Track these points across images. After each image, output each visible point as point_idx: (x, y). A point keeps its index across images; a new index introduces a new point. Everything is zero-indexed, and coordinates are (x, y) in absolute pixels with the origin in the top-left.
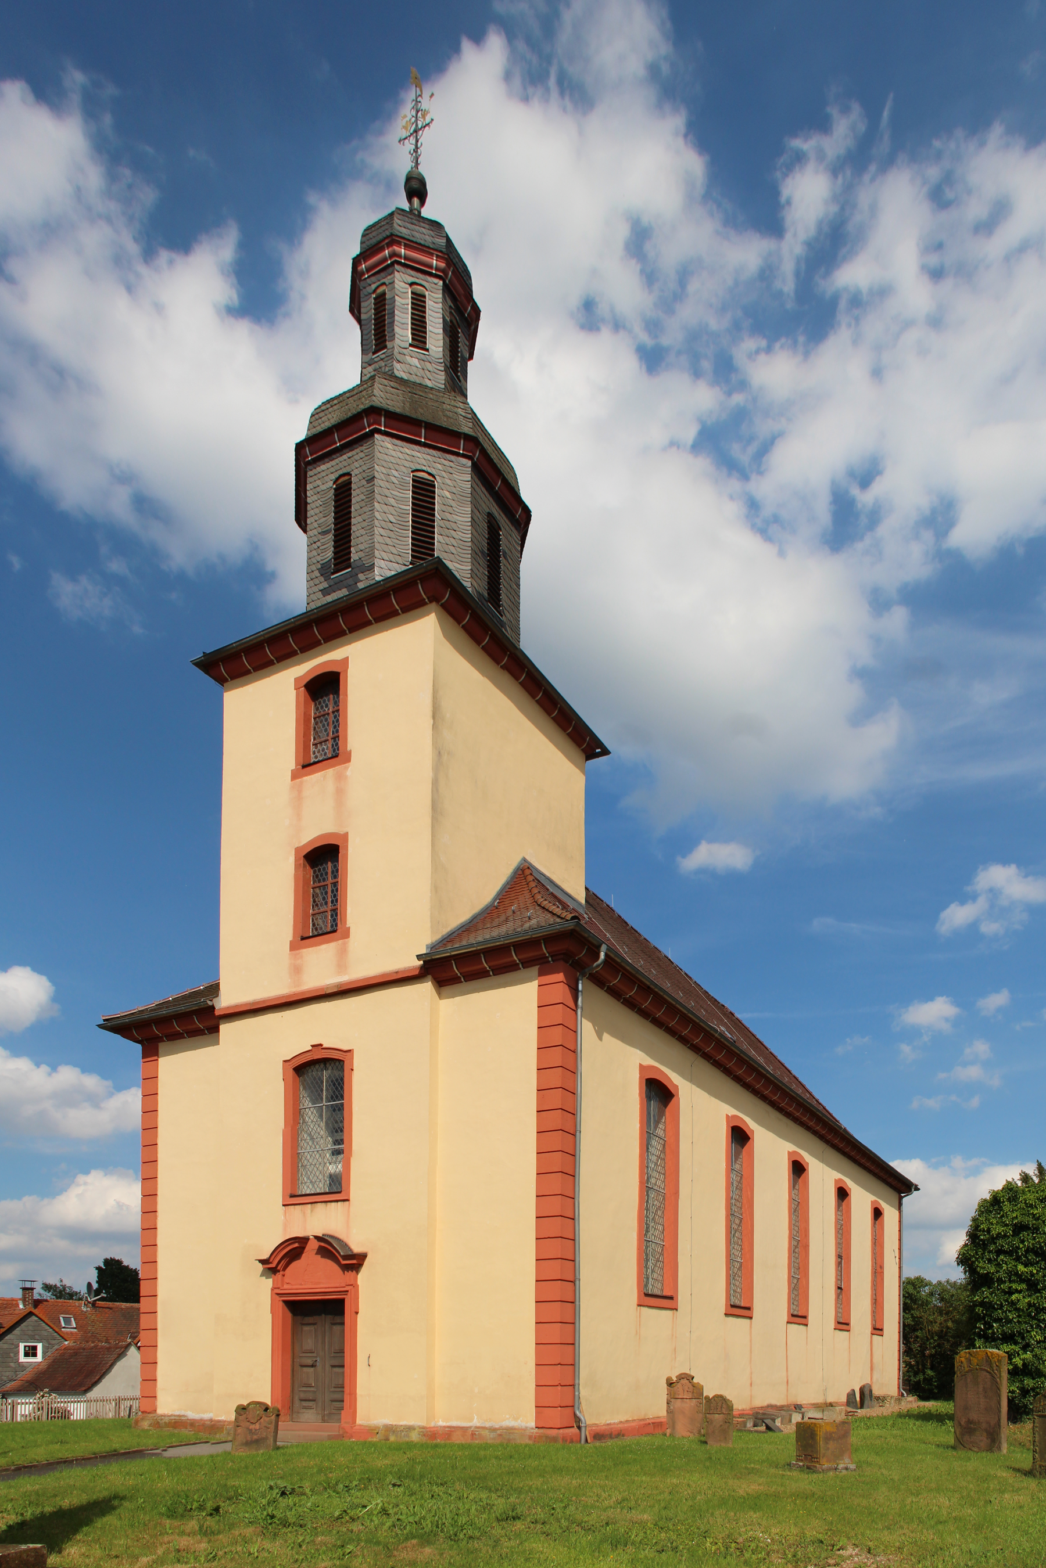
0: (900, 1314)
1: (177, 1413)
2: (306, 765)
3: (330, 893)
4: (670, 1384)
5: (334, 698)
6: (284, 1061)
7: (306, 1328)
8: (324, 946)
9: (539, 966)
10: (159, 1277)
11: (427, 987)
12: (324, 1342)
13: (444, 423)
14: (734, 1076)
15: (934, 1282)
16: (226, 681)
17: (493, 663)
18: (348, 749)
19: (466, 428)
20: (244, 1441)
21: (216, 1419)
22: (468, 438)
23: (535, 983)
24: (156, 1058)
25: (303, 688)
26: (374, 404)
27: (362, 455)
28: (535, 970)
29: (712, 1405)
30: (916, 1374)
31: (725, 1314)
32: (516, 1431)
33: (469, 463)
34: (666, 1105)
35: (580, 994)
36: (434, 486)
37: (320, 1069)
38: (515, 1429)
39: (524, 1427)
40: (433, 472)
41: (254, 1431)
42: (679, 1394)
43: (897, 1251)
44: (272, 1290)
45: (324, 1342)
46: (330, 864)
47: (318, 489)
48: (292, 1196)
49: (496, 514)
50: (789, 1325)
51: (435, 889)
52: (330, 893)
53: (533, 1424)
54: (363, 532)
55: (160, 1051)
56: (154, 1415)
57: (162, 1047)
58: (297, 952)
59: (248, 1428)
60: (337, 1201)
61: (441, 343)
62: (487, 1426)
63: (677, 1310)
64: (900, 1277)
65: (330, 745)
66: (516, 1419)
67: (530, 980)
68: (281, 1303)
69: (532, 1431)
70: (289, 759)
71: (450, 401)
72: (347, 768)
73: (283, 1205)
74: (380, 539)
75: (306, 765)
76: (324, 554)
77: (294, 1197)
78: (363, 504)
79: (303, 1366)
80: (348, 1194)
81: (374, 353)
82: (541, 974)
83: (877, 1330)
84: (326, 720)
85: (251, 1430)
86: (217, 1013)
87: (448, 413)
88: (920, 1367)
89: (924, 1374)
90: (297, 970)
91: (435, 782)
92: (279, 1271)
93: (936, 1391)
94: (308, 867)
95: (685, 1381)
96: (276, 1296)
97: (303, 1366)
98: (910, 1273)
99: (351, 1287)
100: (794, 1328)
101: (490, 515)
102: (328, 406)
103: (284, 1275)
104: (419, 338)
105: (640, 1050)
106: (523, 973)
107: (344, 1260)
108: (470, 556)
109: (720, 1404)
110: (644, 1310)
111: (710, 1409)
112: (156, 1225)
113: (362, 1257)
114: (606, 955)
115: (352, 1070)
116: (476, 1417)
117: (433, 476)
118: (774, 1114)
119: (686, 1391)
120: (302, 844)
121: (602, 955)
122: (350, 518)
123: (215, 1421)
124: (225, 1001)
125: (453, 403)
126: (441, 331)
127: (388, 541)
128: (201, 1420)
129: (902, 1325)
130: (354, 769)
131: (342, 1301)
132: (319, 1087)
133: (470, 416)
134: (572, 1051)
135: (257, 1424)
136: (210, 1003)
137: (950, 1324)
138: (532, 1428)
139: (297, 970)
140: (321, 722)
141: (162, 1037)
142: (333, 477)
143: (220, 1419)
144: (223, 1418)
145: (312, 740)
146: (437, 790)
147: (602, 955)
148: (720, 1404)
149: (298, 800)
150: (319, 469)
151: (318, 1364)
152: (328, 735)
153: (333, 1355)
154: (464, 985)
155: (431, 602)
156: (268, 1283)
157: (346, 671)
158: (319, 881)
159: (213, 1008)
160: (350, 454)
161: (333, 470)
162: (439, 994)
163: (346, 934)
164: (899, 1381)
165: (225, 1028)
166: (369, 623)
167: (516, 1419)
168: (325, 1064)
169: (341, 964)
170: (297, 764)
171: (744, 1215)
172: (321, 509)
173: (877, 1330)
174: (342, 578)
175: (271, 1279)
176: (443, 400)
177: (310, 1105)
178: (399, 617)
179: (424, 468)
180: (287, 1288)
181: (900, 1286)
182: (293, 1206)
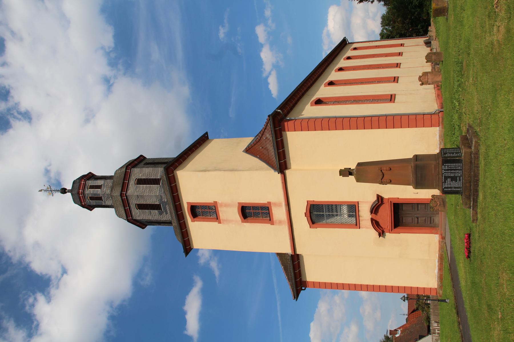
0: (395, 40)
1: (437, 279)
2: (217, 219)
3: (256, 211)
4: (422, 84)
5: (197, 209)
6: (310, 227)
7: (404, 221)
8: (273, 212)
9: (282, 132)
10: (385, 285)
11: (287, 172)
12: (409, 214)
13: (123, 175)
14: (310, 86)
15: (381, 28)
16: (190, 247)
17: (186, 159)
18: (213, 202)
19: (124, 169)
20: (443, 207)
21: (438, 258)
22: (126, 169)
23: (287, 133)
24: (307, 282)
26: (119, 195)
27: (131, 200)
28: (283, 133)
29: (429, 60)
30: (420, 32)
31: (397, 83)
32: (441, 134)
33: (132, 169)
34: (323, 102)
35: (291, 118)
36: (139, 179)
37: (313, 215)
38: (440, 135)
39: (439, 132)
40: (135, 179)
41: (440, 204)
42: (426, 81)
43: (369, 43)
44: (390, 233)
45: (409, 214)
46: (247, 211)
47: (139, 215)
48: (356, 225)
49: (143, 163)
50: (401, 68)
51: (257, 170)
52: (256, 211)
53: (438, 128)
54: (151, 200)
55: (305, 280)
56: (437, 289)
57: (303, 280)
58: (274, 222)
59: (439, 206)
60: (358, 206)
61: (100, 181)
62: (439, 146)
63: (395, 94)
64: (380, 41)
65: (211, 210)
67: (286, 134)
68: (395, 229)
69: (440, 127)
70: (214, 225)
71: (115, 179)
73: (360, 229)
74: (154, 194)
75: (217, 219)
77: (357, 225)
78: (144, 199)
79: (418, 223)
80: (356, 202)
81: (103, 201)
82: (285, 131)
83: (402, 45)
84: (203, 212)
85: (439, 205)
86: (293, 254)
87: (120, 174)
88: (417, 31)
89: (420, 29)
90: (280, 222)
91: (224, 171)
92: (383, 230)
93: (427, 24)
94: (248, 219)
95: (421, 78)
96: (392, 231)
97: (418, 223)
98: (379, 38)
99: (389, 200)
100: (401, 66)
101: (144, 164)
102: (118, 212)
103: (385, 229)
104: (99, 187)
105: (306, 106)
106: (284, 138)
107: (379, 202)
108: (157, 168)
109: (429, 57)
110: (395, 101)
111: (431, 60)
112: (366, 285)
113: (378, 196)
114: (279, 110)
115: (314, 201)
116: (436, 151)
117: (136, 179)
118: (322, 76)
119: (425, 78)
121: (279, 111)
122: (147, 204)
123: (439, 258)
124: (289, 251)
125: (117, 174)
126: (97, 181)
127: (154, 191)
128: (438, 266)
129: (399, 38)
130: (219, 201)
131: (394, 204)
132: (319, 215)
133: (120, 169)
134: (309, 119)
135: (438, 202)
136: (290, 255)
137: (399, 20)
138: (439, 128)
139: (280, 222)
140: (204, 214)
141: (300, 278)
142: (136, 210)
143: (438, 256)
144: (437, 255)
145: (209, 217)
146: (227, 170)
147: (279, 111)
148: (429, 57)
149: (228, 221)
150: (134, 215)
151: (417, 216)
152: (208, 211)
153: (414, 210)
154: (287, 159)
155: (173, 173)
156: (387, 234)
157: (190, 203)
158: (252, 215)
159: (292, 255)
160: (131, 204)
161: (134, 210)
162: (289, 169)
163: (269, 203)
164: (423, 38)
165: (298, 252)
166: (178, 194)
167: (436, 135)
168: (311, 213)
169: (278, 205)
170: (216, 222)
171: (359, 82)
172: (144, 214)
173: (402, 45)
174: (163, 207)
175: (386, 233)
176: (117, 177)
177: (325, 221)
178: (177, 184)
179: (134, 181)
180: (389, 227)
181: (384, 41)
182: (360, 225)
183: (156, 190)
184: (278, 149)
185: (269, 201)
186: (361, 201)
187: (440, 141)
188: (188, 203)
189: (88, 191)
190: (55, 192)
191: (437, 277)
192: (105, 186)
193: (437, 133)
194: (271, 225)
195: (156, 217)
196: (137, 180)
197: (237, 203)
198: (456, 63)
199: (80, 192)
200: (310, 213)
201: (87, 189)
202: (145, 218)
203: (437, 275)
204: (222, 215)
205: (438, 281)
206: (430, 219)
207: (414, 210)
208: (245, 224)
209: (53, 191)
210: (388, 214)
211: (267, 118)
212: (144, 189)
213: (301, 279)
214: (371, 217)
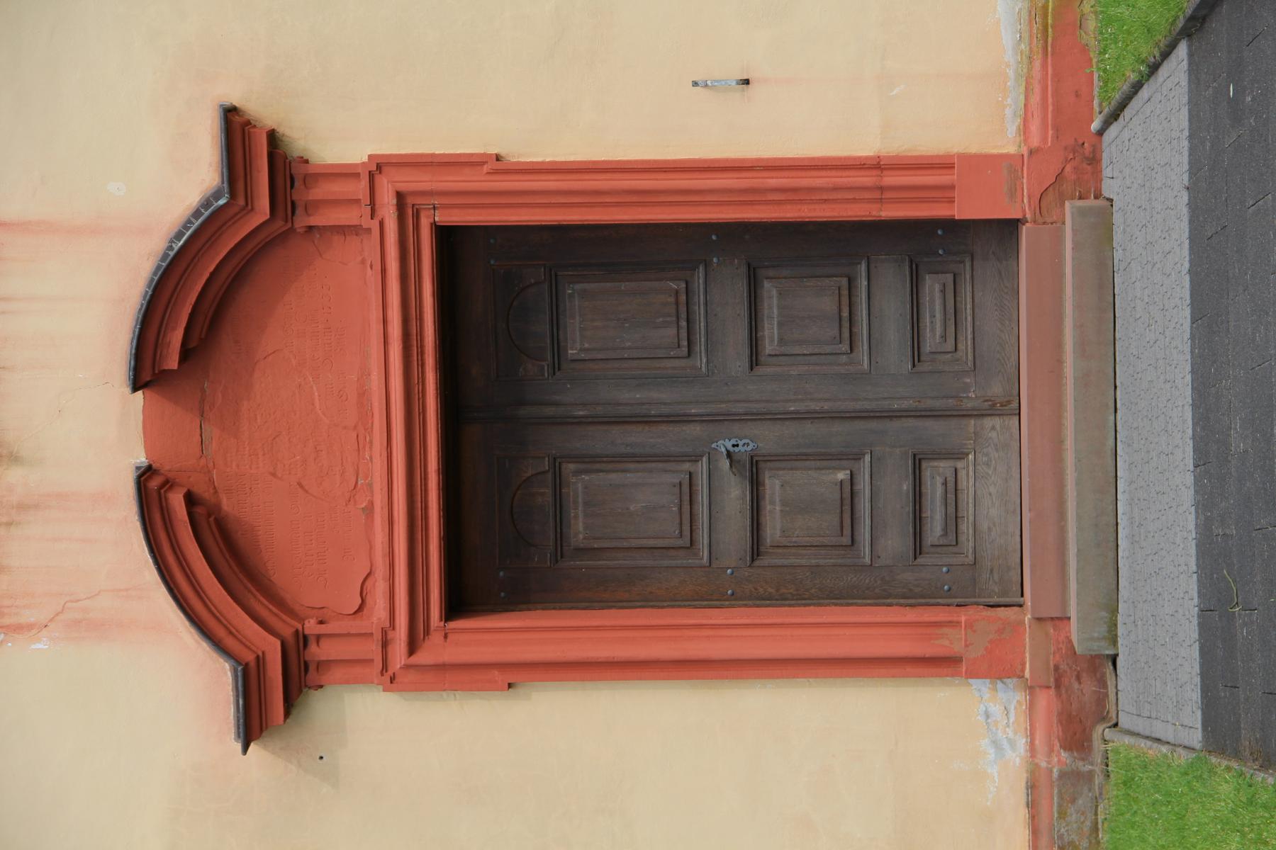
79: (756, 548)
107: (249, 207)
131: (447, 237)
198: (1125, 634)
206: (906, 486)
207: (701, 361)
210: (363, 394)
214: (142, 460)
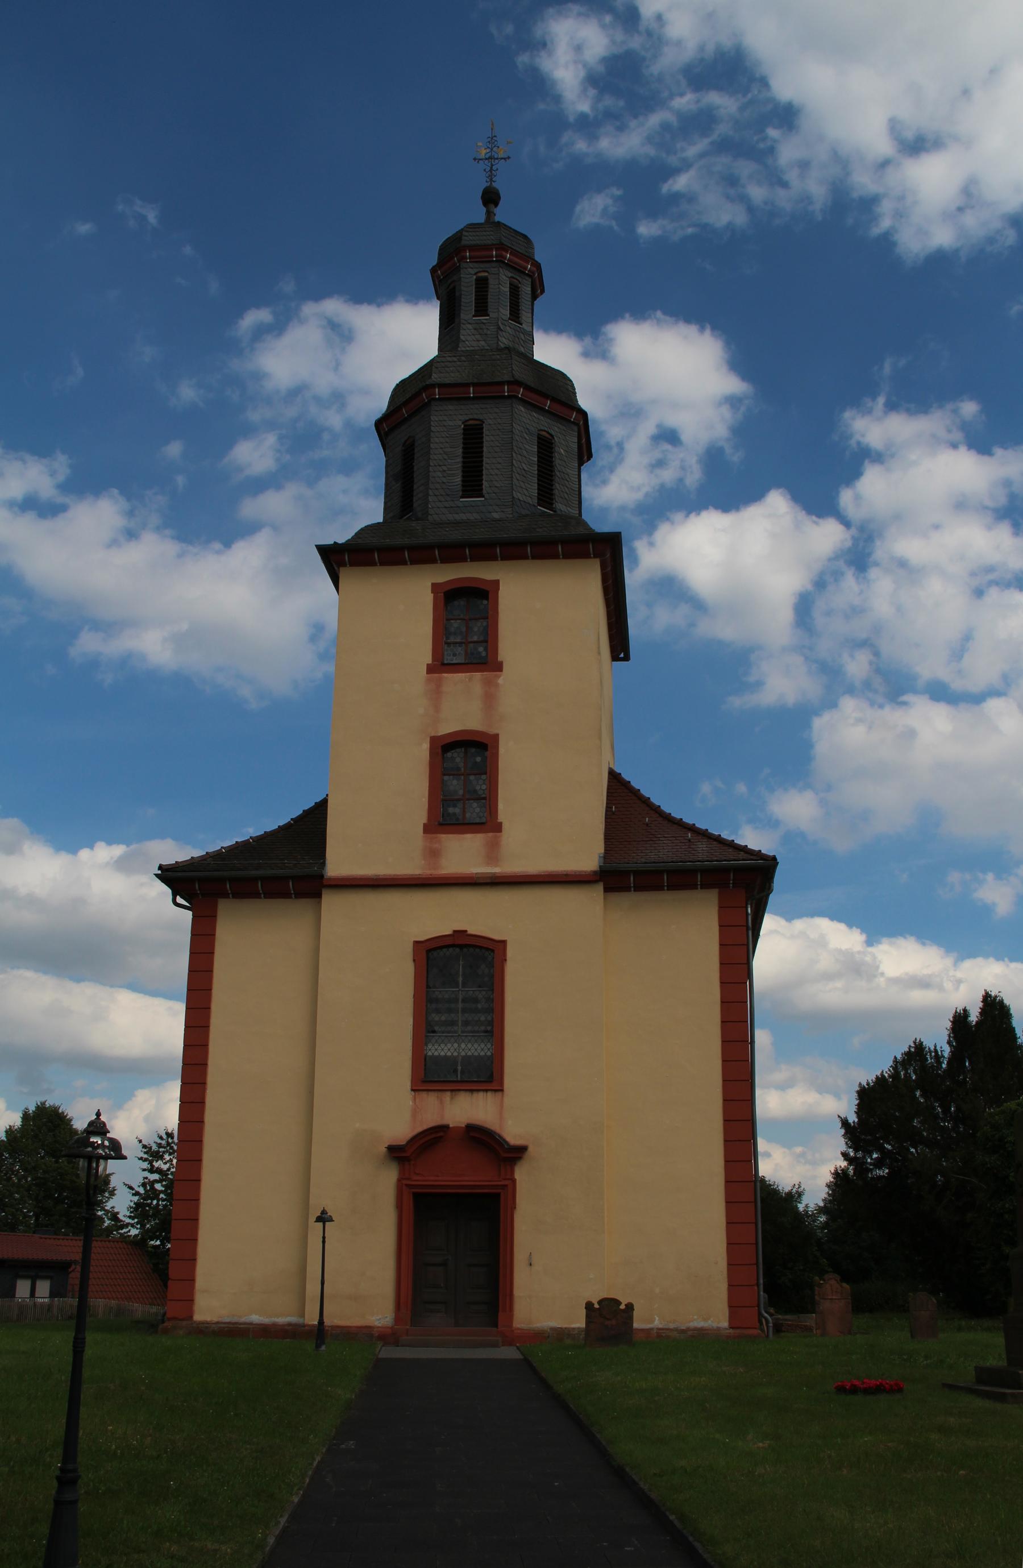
1: (227, 1320)
8: (469, 836)
18: (500, 659)
25: (442, 594)
40: (553, 433)
48: (424, 1082)
53: (725, 1324)
66: (705, 1320)
69: (728, 1331)
72: (499, 677)
75: (439, 666)
76: (450, 478)
90: (433, 854)
113: (520, 1152)
116: (657, 1318)
120: (439, 735)
127: (522, 484)
131: (498, 1195)
139: (433, 854)
149: (436, 695)
155: (595, 557)
167: (705, 1320)
179: (546, 429)
182: (425, 1092)
183: (526, 492)
184: (671, 872)
185: (505, 827)
186: (506, 1100)
187: (688, 1329)
188: (497, 583)
189: (504, 277)
190: (488, 169)
191: (235, 1320)
192: (517, 333)
193: (712, 1322)
194: (424, 824)
195: (439, 474)
196: (550, 438)
197: (495, 731)
199: (504, 253)
200: (461, 947)
201: (510, 275)
202: (437, 440)
203: (243, 1320)
204: (454, 681)
205: (218, 1323)
208: (426, 746)
209: (489, 164)
211: (762, 852)
212: (528, 456)
213: (225, 895)
